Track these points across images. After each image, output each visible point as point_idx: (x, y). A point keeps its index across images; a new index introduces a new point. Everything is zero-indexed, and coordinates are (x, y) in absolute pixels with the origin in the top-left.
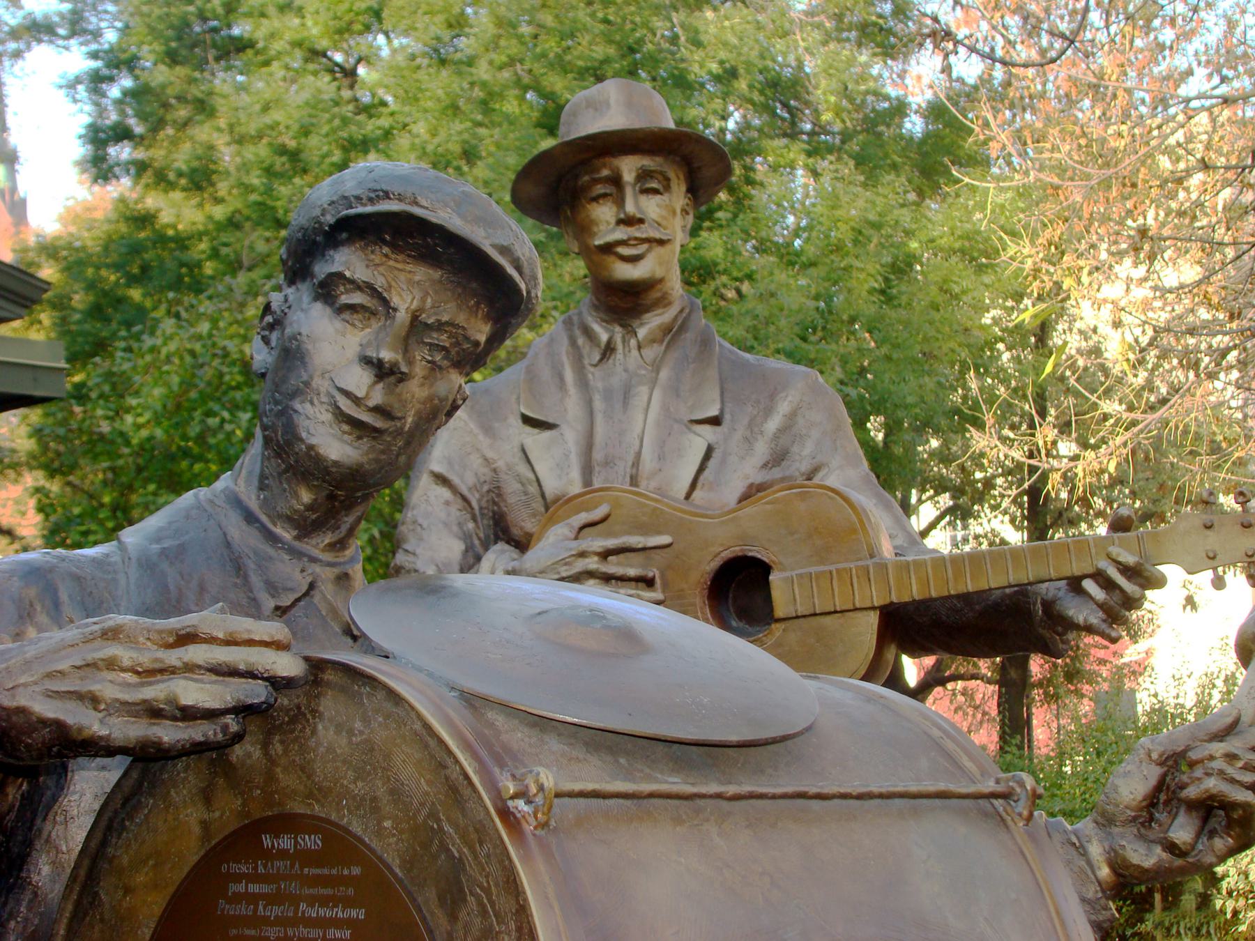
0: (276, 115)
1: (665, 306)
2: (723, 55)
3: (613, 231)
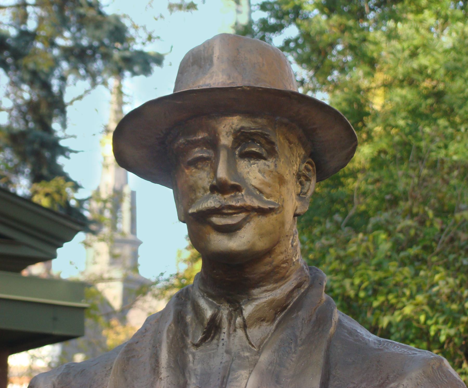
0: (423, 60)
1: (276, 281)
3: (208, 198)
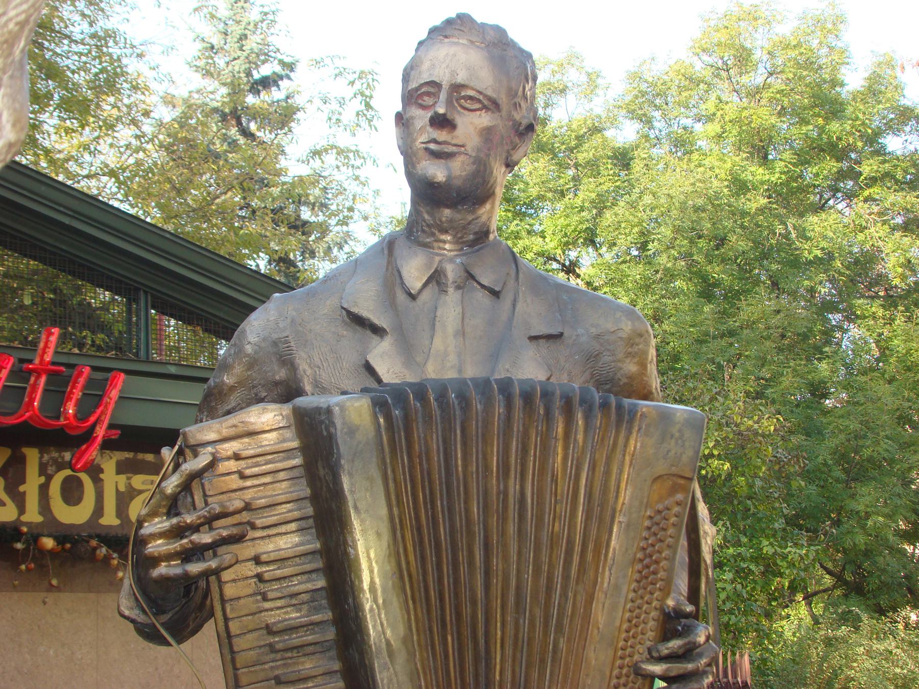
2: (824, 244)
